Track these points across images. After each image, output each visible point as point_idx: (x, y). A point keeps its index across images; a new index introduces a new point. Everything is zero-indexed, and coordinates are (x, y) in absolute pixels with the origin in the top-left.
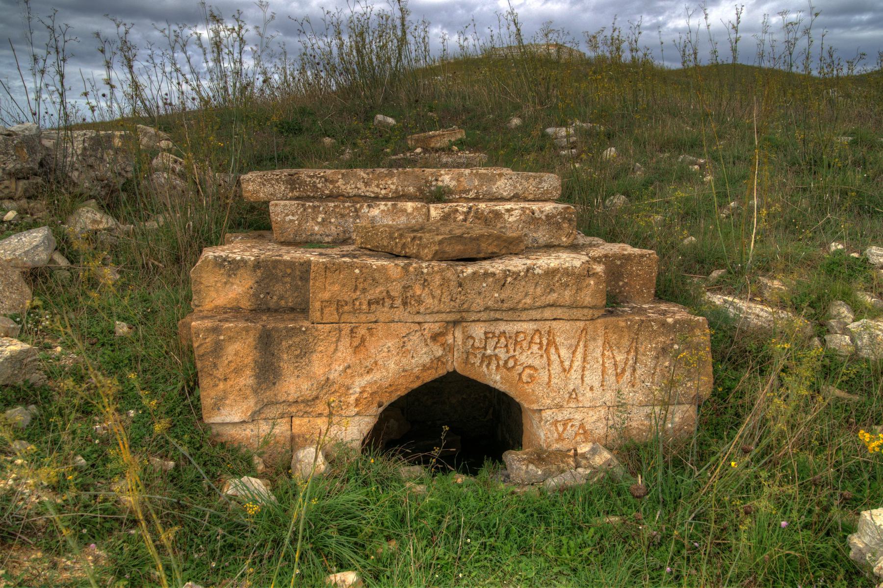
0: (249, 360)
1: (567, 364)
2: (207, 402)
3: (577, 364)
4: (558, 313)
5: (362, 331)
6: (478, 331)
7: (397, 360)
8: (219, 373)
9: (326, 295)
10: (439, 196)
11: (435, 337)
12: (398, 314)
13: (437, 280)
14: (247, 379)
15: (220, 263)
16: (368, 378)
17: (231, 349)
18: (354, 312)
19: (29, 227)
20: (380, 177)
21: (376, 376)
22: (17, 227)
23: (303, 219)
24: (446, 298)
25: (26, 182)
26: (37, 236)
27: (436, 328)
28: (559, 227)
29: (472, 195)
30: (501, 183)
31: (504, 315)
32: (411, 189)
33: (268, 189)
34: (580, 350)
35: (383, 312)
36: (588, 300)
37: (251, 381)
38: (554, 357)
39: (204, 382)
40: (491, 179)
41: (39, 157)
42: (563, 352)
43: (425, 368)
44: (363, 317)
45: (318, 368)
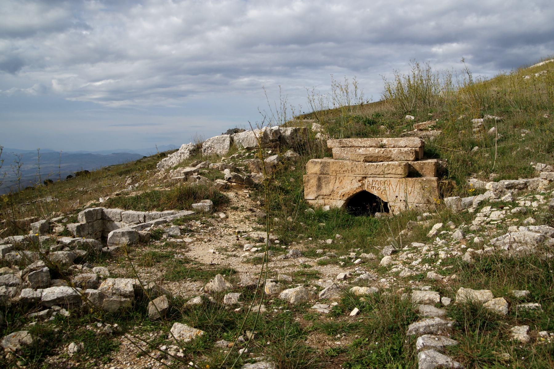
0: (315, 184)
1: (394, 190)
2: (305, 194)
3: (397, 190)
4: (392, 176)
5: (341, 178)
6: (371, 180)
7: (351, 186)
8: (308, 187)
9: (333, 169)
10: (382, 146)
11: (359, 181)
12: (350, 174)
13: (360, 166)
14: (315, 189)
15: (312, 162)
16: (343, 190)
17: (312, 181)
18: (340, 173)
19: (274, 155)
20: (365, 141)
21: (345, 190)
22: (271, 155)
23: (341, 153)
24: (362, 171)
25: (37, 265)
26: (275, 157)
27: (360, 178)
28: (409, 154)
29: (392, 146)
30: (401, 142)
31: (377, 176)
32: (374, 144)
33: (334, 144)
34: (398, 186)
35: (346, 174)
36: (399, 173)
37: (316, 189)
38: (391, 188)
39: (305, 189)
40: (398, 141)
41: (278, 136)
42: (393, 186)
43: (357, 189)
44: (342, 175)
45: (331, 187)
